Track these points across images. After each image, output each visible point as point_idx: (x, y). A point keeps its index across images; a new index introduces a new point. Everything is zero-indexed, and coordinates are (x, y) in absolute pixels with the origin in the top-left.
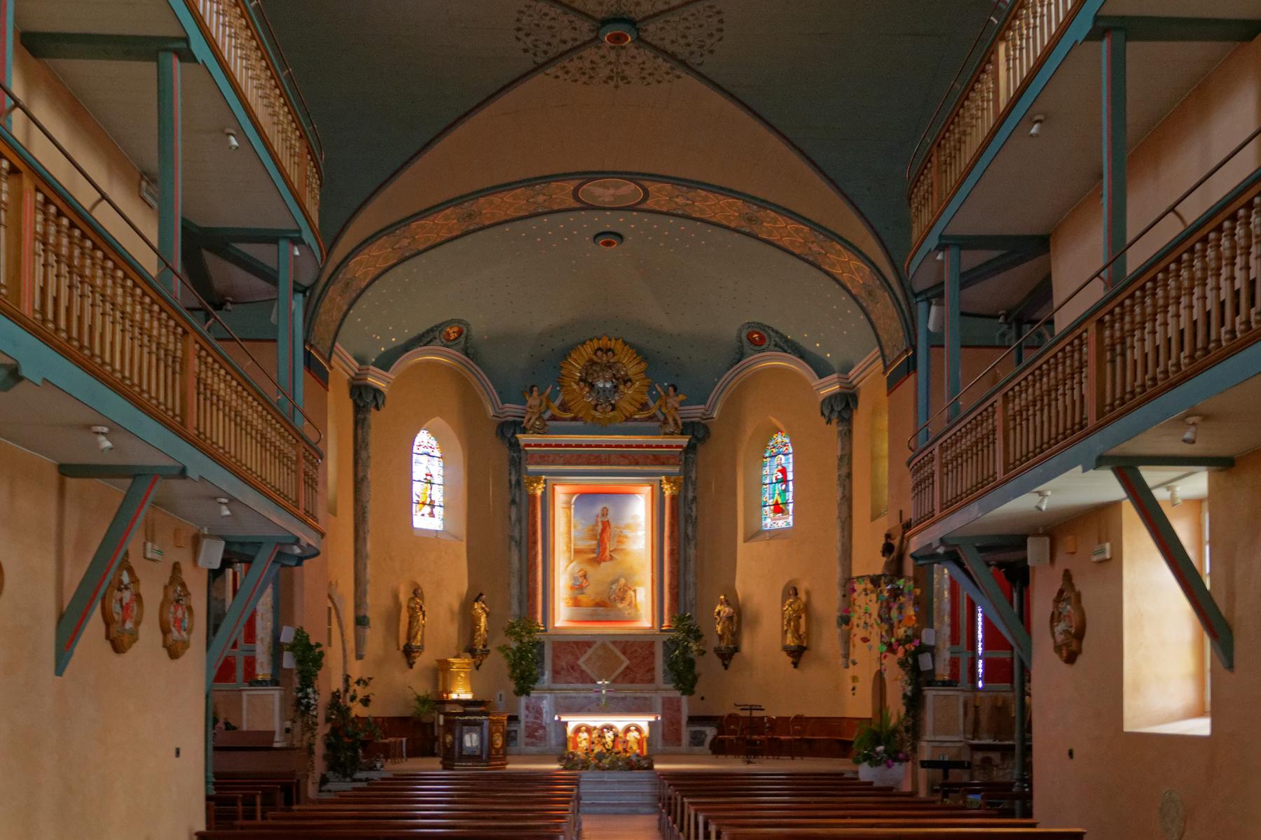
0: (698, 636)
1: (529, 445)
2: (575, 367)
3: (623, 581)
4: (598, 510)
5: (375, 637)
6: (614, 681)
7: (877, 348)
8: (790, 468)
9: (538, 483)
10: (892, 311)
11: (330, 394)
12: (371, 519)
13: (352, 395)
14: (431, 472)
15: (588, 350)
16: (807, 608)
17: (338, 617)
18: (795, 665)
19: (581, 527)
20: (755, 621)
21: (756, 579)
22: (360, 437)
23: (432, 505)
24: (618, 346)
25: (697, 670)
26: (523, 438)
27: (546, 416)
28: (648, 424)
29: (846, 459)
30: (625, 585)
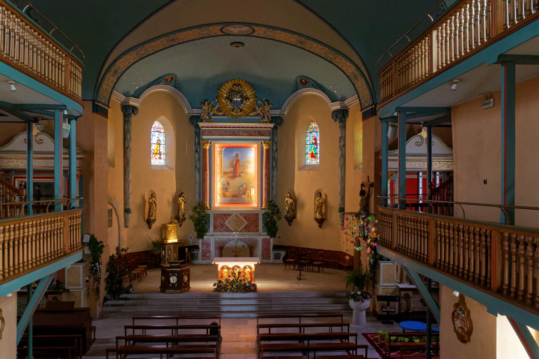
0: (278, 212)
1: (204, 127)
2: (224, 92)
3: (245, 186)
4: (234, 154)
5: (133, 217)
7: (357, 95)
8: (318, 138)
9: (208, 144)
10: (365, 86)
11: (109, 120)
12: (131, 164)
13: (122, 110)
14: (159, 141)
15: (229, 86)
16: (325, 202)
17: (116, 212)
18: (320, 227)
19: (227, 162)
20: (303, 206)
21: (303, 187)
22: (126, 129)
23: (160, 154)
24: (243, 83)
26: (201, 124)
27: (211, 114)
29: (343, 138)
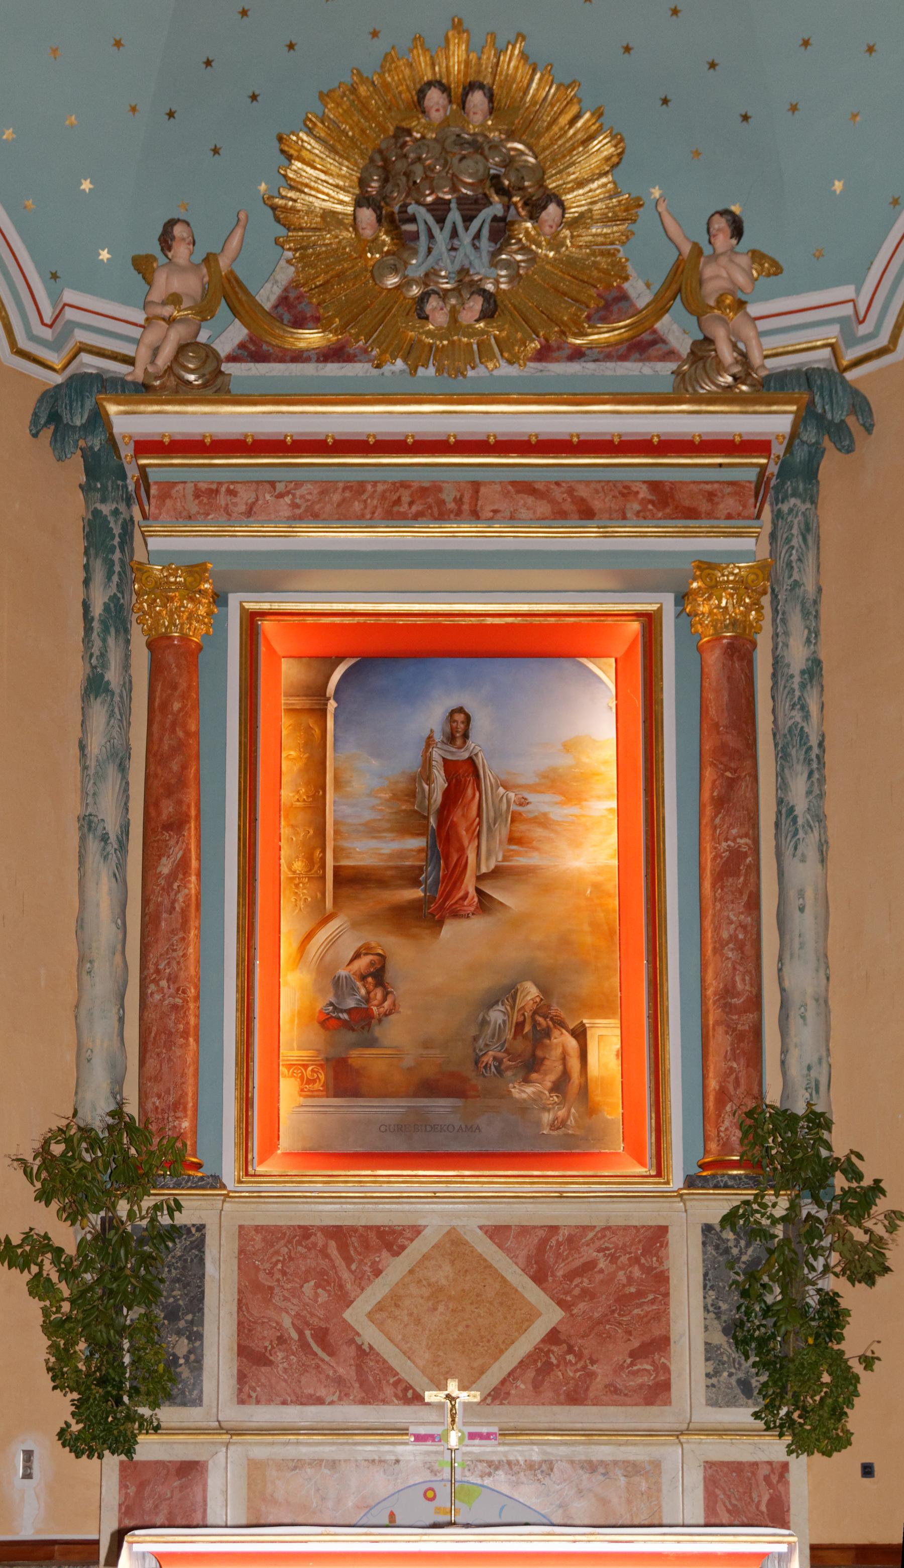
3: (531, 992)
6: (498, 1395)
25: (853, 1343)
28: (631, 368)
30: (541, 1010)
